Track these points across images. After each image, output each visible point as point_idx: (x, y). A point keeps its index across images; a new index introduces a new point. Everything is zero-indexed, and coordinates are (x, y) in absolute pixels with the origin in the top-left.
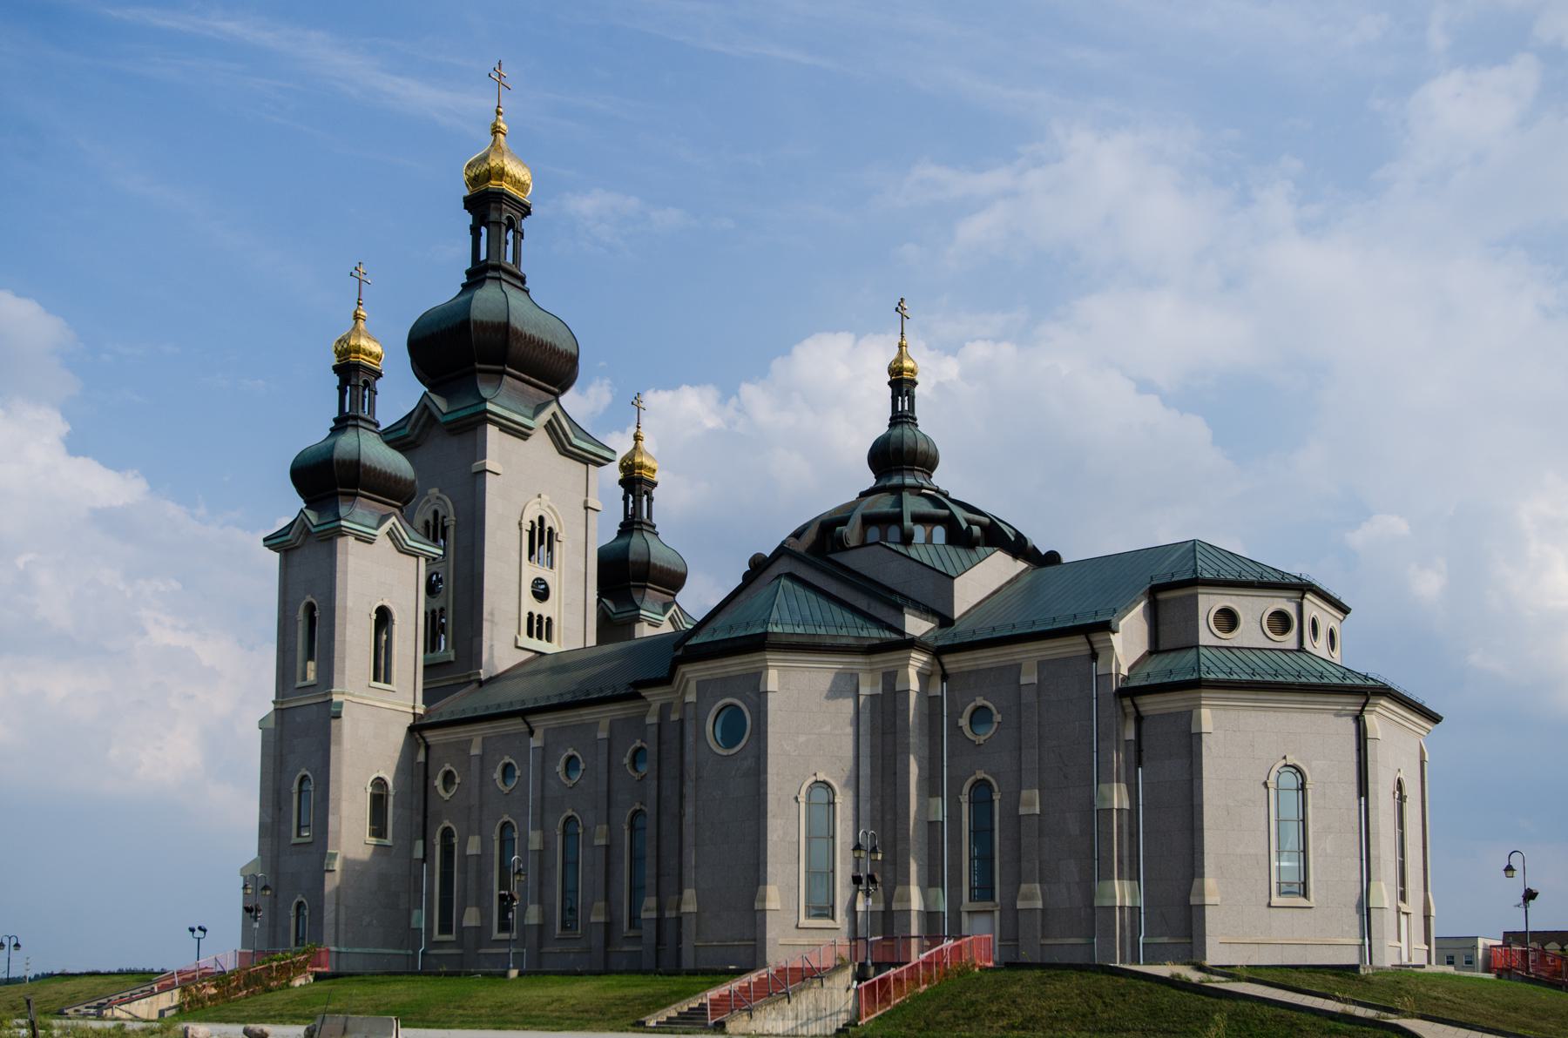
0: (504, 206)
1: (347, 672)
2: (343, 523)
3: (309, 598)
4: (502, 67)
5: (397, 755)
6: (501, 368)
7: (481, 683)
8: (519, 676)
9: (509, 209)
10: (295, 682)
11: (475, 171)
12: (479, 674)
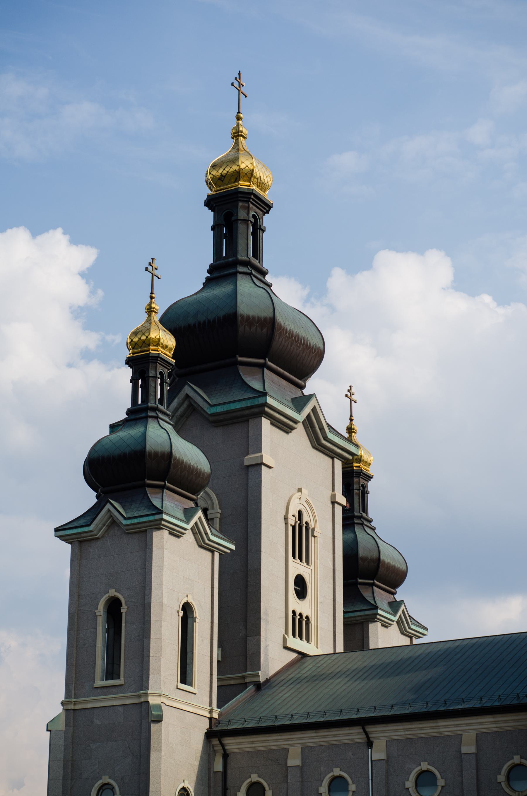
0: (251, 205)
1: (162, 673)
2: (165, 517)
3: (112, 593)
4: (241, 76)
5: (197, 763)
6: (262, 361)
7: (259, 686)
8: (298, 681)
9: (254, 207)
10: (94, 681)
11: (217, 173)
12: (258, 675)
